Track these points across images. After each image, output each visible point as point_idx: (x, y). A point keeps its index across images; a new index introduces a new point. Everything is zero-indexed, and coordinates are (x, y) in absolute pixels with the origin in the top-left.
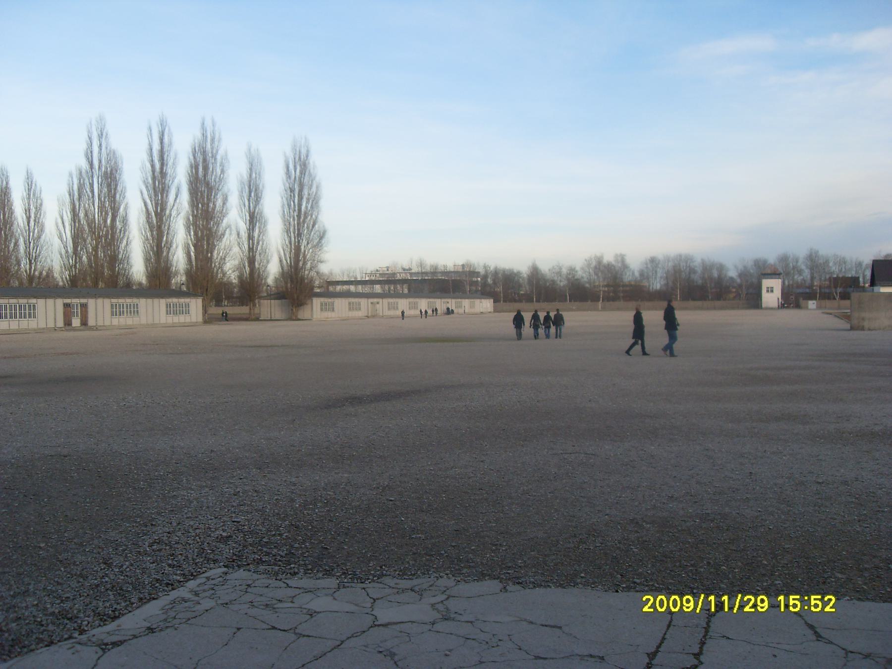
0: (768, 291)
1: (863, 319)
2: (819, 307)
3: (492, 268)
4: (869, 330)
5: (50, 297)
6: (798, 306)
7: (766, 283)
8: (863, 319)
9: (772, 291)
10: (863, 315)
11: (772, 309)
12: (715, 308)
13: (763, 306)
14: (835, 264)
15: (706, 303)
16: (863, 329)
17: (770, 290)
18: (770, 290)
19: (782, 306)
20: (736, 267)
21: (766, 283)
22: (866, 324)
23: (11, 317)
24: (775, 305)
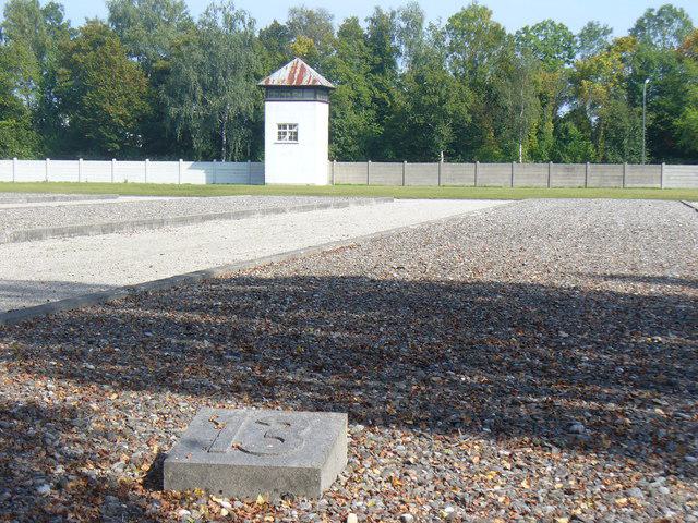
0: (281, 135)
17: (289, 132)
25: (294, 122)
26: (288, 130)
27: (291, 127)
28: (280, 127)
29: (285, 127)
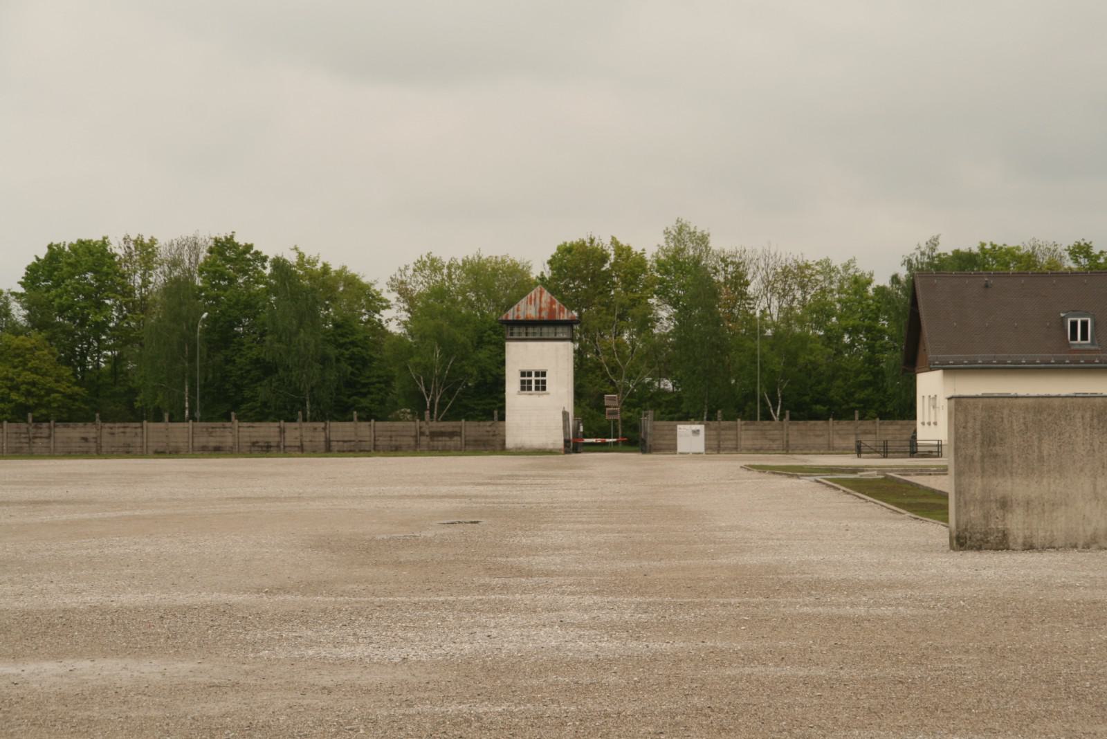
0: (525, 386)
1: (1004, 504)
2: (715, 447)
3: (950, 254)
4: (1029, 547)
5: (516, 321)
6: (634, 441)
7: (521, 356)
8: (1004, 504)
9: (541, 386)
10: (1006, 486)
11: (551, 452)
12: (328, 449)
13: (510, 443)
14: (769, 286)
15: (295, 431)
16: (1002, 543)
17: (535, 382)
18: (535, 382)
19: (573, 446)
20: (402, 290)
21: (521, 356)
22: (1016, 524)
23: (537, 389)
24: (556, 438)
25: (540, 368)
26: (533, 378)
27: (537, 374)
28: (523, 374)
29: (530, 374)
